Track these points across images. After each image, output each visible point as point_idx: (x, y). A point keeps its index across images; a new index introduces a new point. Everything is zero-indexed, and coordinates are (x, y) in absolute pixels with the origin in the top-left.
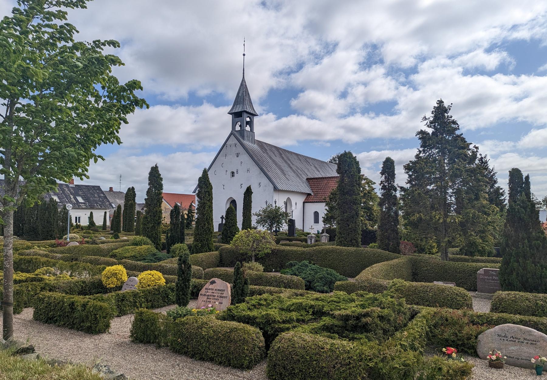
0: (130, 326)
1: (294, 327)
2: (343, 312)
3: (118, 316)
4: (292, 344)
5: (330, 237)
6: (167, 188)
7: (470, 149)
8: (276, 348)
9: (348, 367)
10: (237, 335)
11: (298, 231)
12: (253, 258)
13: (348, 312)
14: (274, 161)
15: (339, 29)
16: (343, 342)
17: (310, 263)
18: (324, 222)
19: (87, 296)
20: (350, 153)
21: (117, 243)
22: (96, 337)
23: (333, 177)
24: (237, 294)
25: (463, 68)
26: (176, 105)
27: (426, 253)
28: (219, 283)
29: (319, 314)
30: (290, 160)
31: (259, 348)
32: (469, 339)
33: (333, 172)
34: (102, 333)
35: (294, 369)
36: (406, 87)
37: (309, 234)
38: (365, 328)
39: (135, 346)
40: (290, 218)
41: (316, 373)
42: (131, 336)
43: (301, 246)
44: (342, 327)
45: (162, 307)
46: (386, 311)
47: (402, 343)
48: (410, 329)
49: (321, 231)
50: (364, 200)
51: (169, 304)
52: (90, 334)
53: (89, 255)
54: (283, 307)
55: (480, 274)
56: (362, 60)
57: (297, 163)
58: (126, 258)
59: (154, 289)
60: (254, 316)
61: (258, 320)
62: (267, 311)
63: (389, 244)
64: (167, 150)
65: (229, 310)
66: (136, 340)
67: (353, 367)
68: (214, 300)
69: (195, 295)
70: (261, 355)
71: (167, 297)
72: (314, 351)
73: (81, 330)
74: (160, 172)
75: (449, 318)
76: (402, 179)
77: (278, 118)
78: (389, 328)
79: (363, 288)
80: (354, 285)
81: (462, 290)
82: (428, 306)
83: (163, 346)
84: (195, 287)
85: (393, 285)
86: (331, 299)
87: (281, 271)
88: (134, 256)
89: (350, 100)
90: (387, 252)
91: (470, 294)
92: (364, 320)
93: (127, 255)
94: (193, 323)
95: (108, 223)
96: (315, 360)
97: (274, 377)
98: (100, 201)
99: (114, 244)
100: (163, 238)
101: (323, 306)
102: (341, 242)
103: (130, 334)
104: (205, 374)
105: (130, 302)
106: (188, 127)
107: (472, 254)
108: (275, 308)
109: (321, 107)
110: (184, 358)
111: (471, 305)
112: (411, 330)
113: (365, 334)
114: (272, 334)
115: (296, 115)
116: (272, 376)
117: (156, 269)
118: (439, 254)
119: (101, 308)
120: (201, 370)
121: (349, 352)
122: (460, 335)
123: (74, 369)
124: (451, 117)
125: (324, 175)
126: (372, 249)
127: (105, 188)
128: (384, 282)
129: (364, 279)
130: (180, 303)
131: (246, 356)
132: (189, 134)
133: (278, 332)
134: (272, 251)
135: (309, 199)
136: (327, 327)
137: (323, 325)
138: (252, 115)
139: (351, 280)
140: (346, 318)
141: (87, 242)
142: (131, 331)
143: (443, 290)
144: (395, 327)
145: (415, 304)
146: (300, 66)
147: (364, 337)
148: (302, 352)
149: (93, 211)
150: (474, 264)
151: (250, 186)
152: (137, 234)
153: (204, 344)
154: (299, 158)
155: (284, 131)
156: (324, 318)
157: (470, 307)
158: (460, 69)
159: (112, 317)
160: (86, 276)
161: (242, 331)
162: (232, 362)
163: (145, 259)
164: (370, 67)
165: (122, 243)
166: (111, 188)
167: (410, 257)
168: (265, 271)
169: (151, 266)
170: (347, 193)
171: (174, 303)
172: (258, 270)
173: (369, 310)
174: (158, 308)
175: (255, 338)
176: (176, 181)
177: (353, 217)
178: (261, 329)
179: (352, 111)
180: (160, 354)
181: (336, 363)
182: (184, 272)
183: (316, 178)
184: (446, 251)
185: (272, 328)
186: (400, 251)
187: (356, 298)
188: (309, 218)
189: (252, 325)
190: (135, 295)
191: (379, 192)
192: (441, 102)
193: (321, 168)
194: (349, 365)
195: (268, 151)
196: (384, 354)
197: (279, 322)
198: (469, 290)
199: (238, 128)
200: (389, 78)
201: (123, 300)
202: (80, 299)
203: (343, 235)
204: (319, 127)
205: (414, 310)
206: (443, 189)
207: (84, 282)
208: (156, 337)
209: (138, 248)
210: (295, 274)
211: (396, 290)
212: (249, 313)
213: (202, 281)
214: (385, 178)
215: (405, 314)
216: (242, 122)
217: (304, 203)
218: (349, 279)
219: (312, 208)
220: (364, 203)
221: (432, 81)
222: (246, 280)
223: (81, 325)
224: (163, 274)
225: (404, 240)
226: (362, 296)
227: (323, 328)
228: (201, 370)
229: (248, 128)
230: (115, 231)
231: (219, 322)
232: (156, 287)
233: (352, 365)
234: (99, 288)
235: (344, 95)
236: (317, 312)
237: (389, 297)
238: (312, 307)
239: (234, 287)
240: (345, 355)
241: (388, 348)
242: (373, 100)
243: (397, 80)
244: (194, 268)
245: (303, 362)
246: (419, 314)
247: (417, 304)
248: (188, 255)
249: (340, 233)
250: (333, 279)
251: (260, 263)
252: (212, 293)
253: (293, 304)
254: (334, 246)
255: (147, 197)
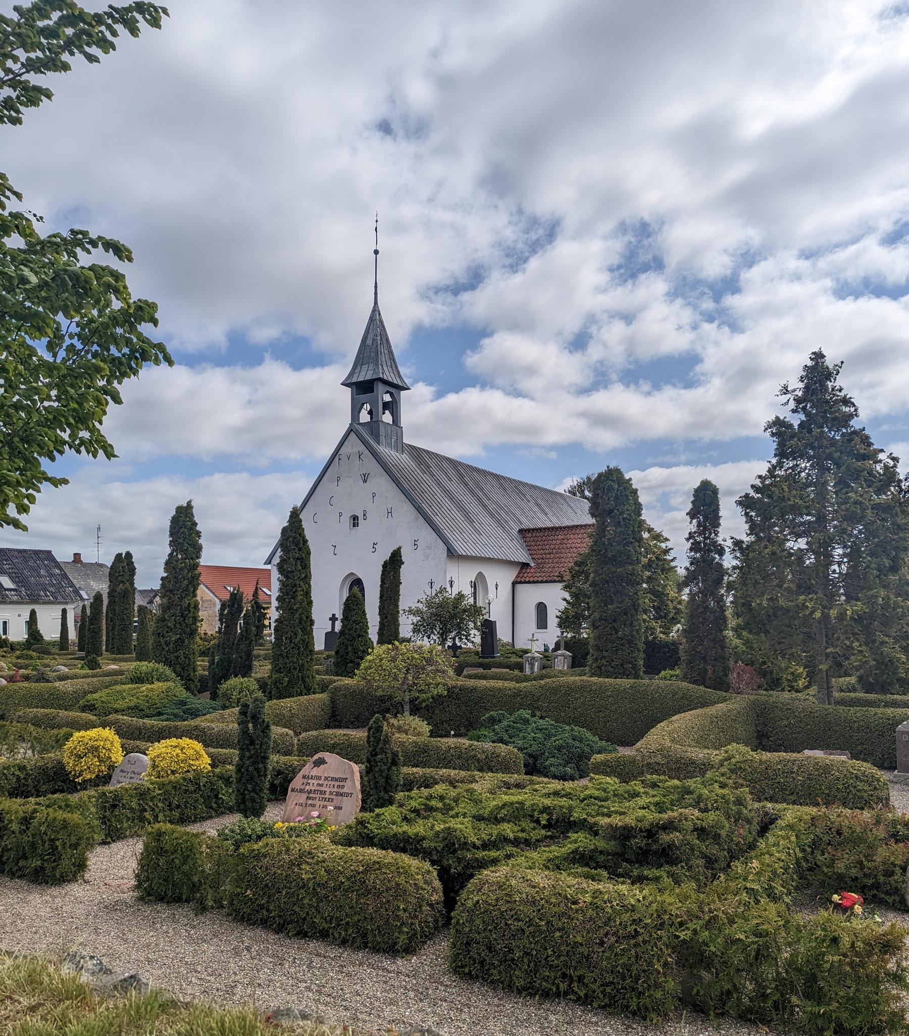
0: (134, 864)
1: (508, 857)
2: (616, 820)
3: (104, 843)
4: (507, 895)
5: (573, 658)
6: (211, 556)
7: (880, 461)
8: (470, 904)
9: (632, 942)
10: (382, 877)
11: (503, 646)
12: (407, 707)
13: (629, 820)
14: (447, 492)
15: (558, 188)
16: (620, 887)
17: (533, 715)
18: (560, 625)
19: (32, 800)
20: (618, 471)
21: (95, 679)
22: (55, 891)
23: (577, 526)
24: (376, 787)
25: (838, 280)
26: (204, 365)
27: (783, 690)
28: (334, 763)
29: (560, 825)
30: (482, 490)
31: (431, 905)
32: (889, 874)
33: (581, 514)
34: (69, 881)
35: (511, 951)
36: (714, 325)
37: (526, 652)
38: (666, 856)
39: (147, 910)
40: (486, 617)
41: (562, 958)
42: (138, 887)
43: (512, 680)
44: (614, 854)
45: (204, 819)
46: (712, 816)
47: (748, 885)
48: (762, 854)
49: (552, 646)
50: (648, 573)
51: (220, 814)
52: (40, 884)
53: (30, 707)
54: (481, 812)
55: (903, 733)
56: (616, 260)
57: (497, 495)
58: (116, 711)
59: (184, 779)
60: (417, 835)
61: (425, 844)
62: (445, 822)
63: (706, 670)
64: (193, 467)
65: (361, 823)
66: (149, 895)
67: (645, 942)
68: (322, 803)
69: (280, 792)
70: (436, 921)
71: (216, 796)
72: (555, 909)
73: (19, 877)
74: (196, 519)
75: (845, 830)
76: (733, 525)
77: (439, 395)
78: (718, 856)
79: (655, 769)
80: (633, 761)
81: (867, 767)
82: (794, 803)
83: (212, 908)
84: (279, 773)
85: (726, 760)
86: (587, 792)
87: (470, 734)
88: (136, 707)
89: (595, 353)
90: (702, 688)
91: (884, 776)
92: (665, 838)
93: (120, 704)
94: (279, 853)
95: (72, 635)
96: (559, 930)
97: (467, 970)
98: (53, 585)
99: (88, 680)
100: (202, 666)
101: (570, 809)
102: (599, 667)
103: (134, 882)
104: (310, 967)
105: (132, 810)
106: (236, 416)
107: (884, 688)
108: (465, 815)
109: (531, 370)
110: (260, 932)
111: (888, 799)
112: (767, 856)
113: (667, 867)
114: (460, 874)
115: (478, 388)
116: (462, 967)
117: (189, 733)
118: (813, 690)
119: (65, 825)
120: (301, 959)
121: (633, 909)
122: (870, 865)
123: (18, 967)
124: (840, 390)
125: (557, 523)
126: (667, 681)
127: (63, 554)
128: (699, 754)
129: (654, 747)
130: (246, 811)
131: (403, 924)
132: (239, 431)
133: (473, 868)
134: (448, 690)
135: (525, 575)
136: (582, 856)
137: (573, 852)
138: (397, 388)
139: (625, 752)
140: (624, 834)
141: (27, 678)
142: (137, 876)
143: (826, 769)
144: (729, 851)
145: (766, 799)
146: (475, 278)
147: (665, 875)
148: (528, 910)
149: (36, 607)
150: (889, 711)
151: (399, 548)
152: (140, 658)
153: (306, 901)
154: (501, 485)
155: (453, 422)
156: (573, 836)
157: (885, 802)
158: (828, 283)
159: (90, 846)
160: (25, 754)
161: (393, 868)
162: (370, 938)
163: (160, 714)
164: (634, 276)
165: (108, 678)
166: (77, 556)
167: (752, 697)
168: (433, 734)
169: (176, 728)
170: (614, 559)
171: (231, 810)
172: (419, 734)
173: (675, 814)
174: (195, 822)
175: (421, 883)
176: (224, 538)
177: (625, 614)
178: (433, 863)
179: (600, 379)
180: (206, 926)
181: (606, 935)
182: (253, 741)
183: (541, 529)
184: (828, 683)
185: (459, 860)
186: (728, 685)
187: (642, 790)
188: (529, 618)
189: (414, 853)
190: (142, 794)
191: (681, 559)
192: (818, 356)
193: (550, 507)
194: (634, 937)
195: (434, 469)
196: (710, 911)
197: (474, 846)
198: (881, 767)
199: (364, 417)
200: (679, 301)
201: (114, 806)
202: (15, 807)
203: (605, 654)
204: (532, 417)
205: (766, 814)
206: (822, 550)
207: (22, 768)
208: (194, 888)
209: (144, 688)
210: (501, 741)
211: (732, 771)
212: (406, 828)
213: (294, 760)
214: (699, 525)
215: (749, 821)
216: (374, 404)
217: (514, 584)
218: (620, 749)
219: (531, 595)
220: (649, 580)
221: (768, 310)
222: (395, 755)
223: (21, 864)
224: (206, 745)
225: (736, 662)
226: (654, 785)
227: (574, 858)
228: (301, 959)
229: (387, 418)
230: (88, 653)
231: (340, 850)
232: (190, 775)
233: (640, 938)
234: (59, 780)
235: (579, 343)
236: (557, 821)
237: (716, 785)
238: (545, 809)
239: (369, 771)
240: (626, 917)
241: (719, 898)
242: (645, 353)
243: (695, 308)
244: (277, 731)
245: (533, 935)
246: (779, 821)
247: (771, 799)
248: (262, 702)
249: (598, 648)
250: (586, 749)
251: (424, 717)
252: (319, 785)
253: (504, 805)
254: (585, 678)
255: (165, 575)
